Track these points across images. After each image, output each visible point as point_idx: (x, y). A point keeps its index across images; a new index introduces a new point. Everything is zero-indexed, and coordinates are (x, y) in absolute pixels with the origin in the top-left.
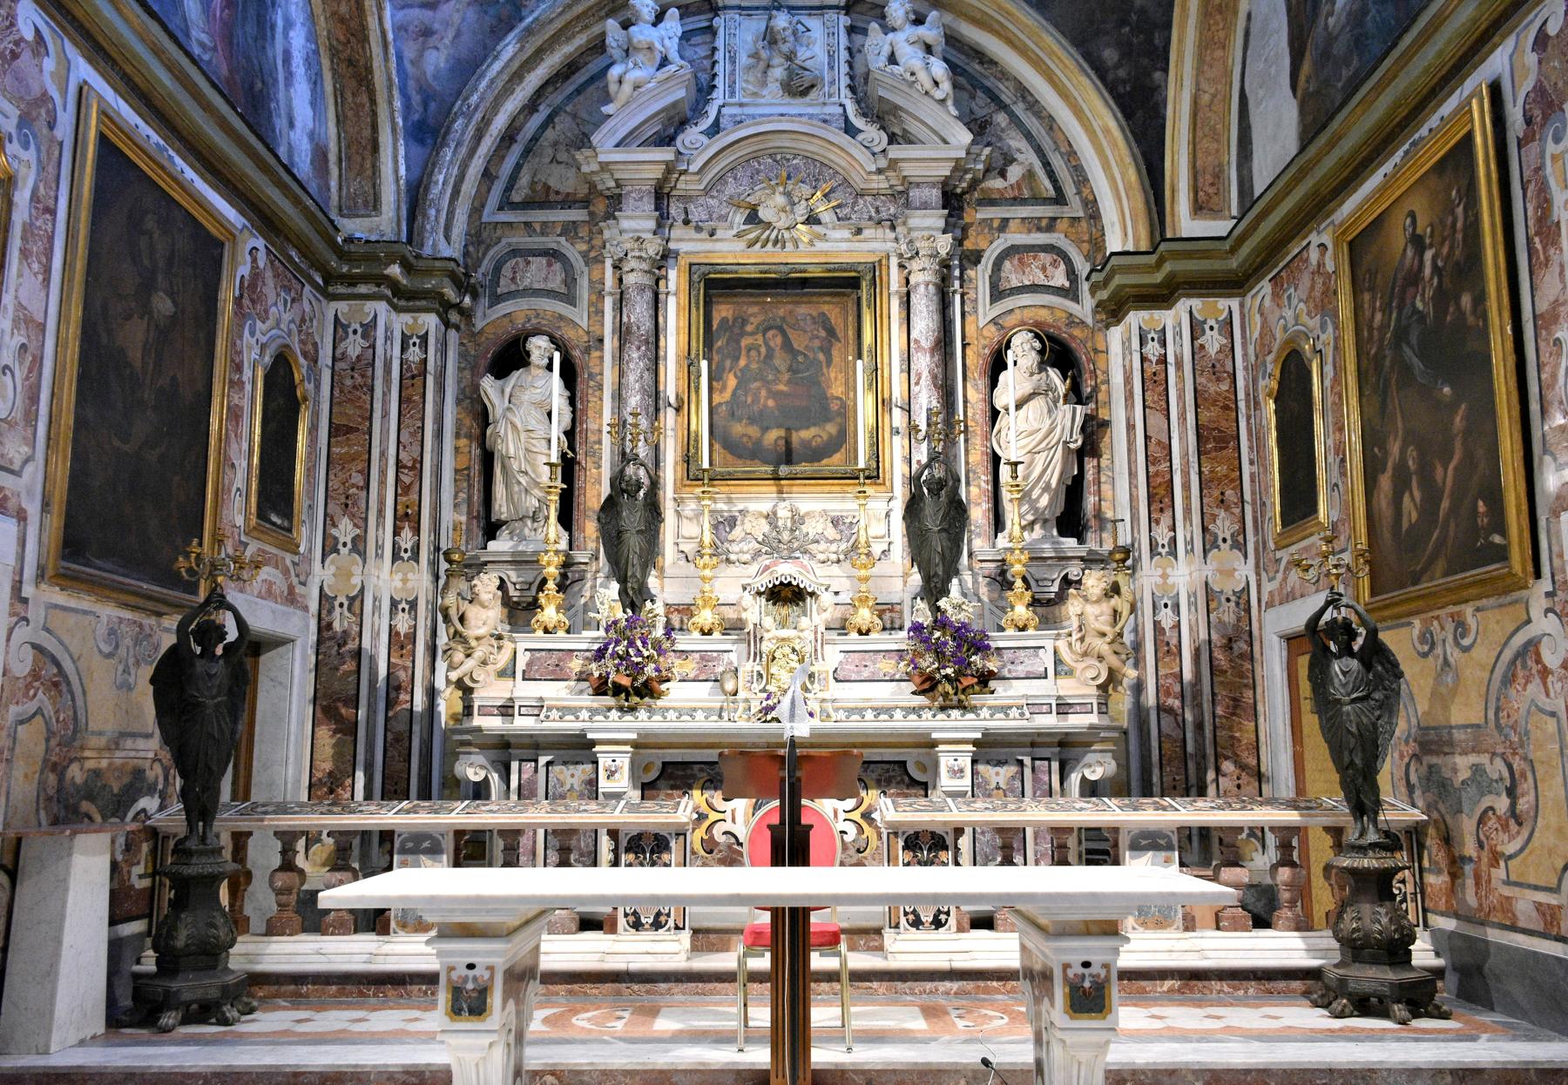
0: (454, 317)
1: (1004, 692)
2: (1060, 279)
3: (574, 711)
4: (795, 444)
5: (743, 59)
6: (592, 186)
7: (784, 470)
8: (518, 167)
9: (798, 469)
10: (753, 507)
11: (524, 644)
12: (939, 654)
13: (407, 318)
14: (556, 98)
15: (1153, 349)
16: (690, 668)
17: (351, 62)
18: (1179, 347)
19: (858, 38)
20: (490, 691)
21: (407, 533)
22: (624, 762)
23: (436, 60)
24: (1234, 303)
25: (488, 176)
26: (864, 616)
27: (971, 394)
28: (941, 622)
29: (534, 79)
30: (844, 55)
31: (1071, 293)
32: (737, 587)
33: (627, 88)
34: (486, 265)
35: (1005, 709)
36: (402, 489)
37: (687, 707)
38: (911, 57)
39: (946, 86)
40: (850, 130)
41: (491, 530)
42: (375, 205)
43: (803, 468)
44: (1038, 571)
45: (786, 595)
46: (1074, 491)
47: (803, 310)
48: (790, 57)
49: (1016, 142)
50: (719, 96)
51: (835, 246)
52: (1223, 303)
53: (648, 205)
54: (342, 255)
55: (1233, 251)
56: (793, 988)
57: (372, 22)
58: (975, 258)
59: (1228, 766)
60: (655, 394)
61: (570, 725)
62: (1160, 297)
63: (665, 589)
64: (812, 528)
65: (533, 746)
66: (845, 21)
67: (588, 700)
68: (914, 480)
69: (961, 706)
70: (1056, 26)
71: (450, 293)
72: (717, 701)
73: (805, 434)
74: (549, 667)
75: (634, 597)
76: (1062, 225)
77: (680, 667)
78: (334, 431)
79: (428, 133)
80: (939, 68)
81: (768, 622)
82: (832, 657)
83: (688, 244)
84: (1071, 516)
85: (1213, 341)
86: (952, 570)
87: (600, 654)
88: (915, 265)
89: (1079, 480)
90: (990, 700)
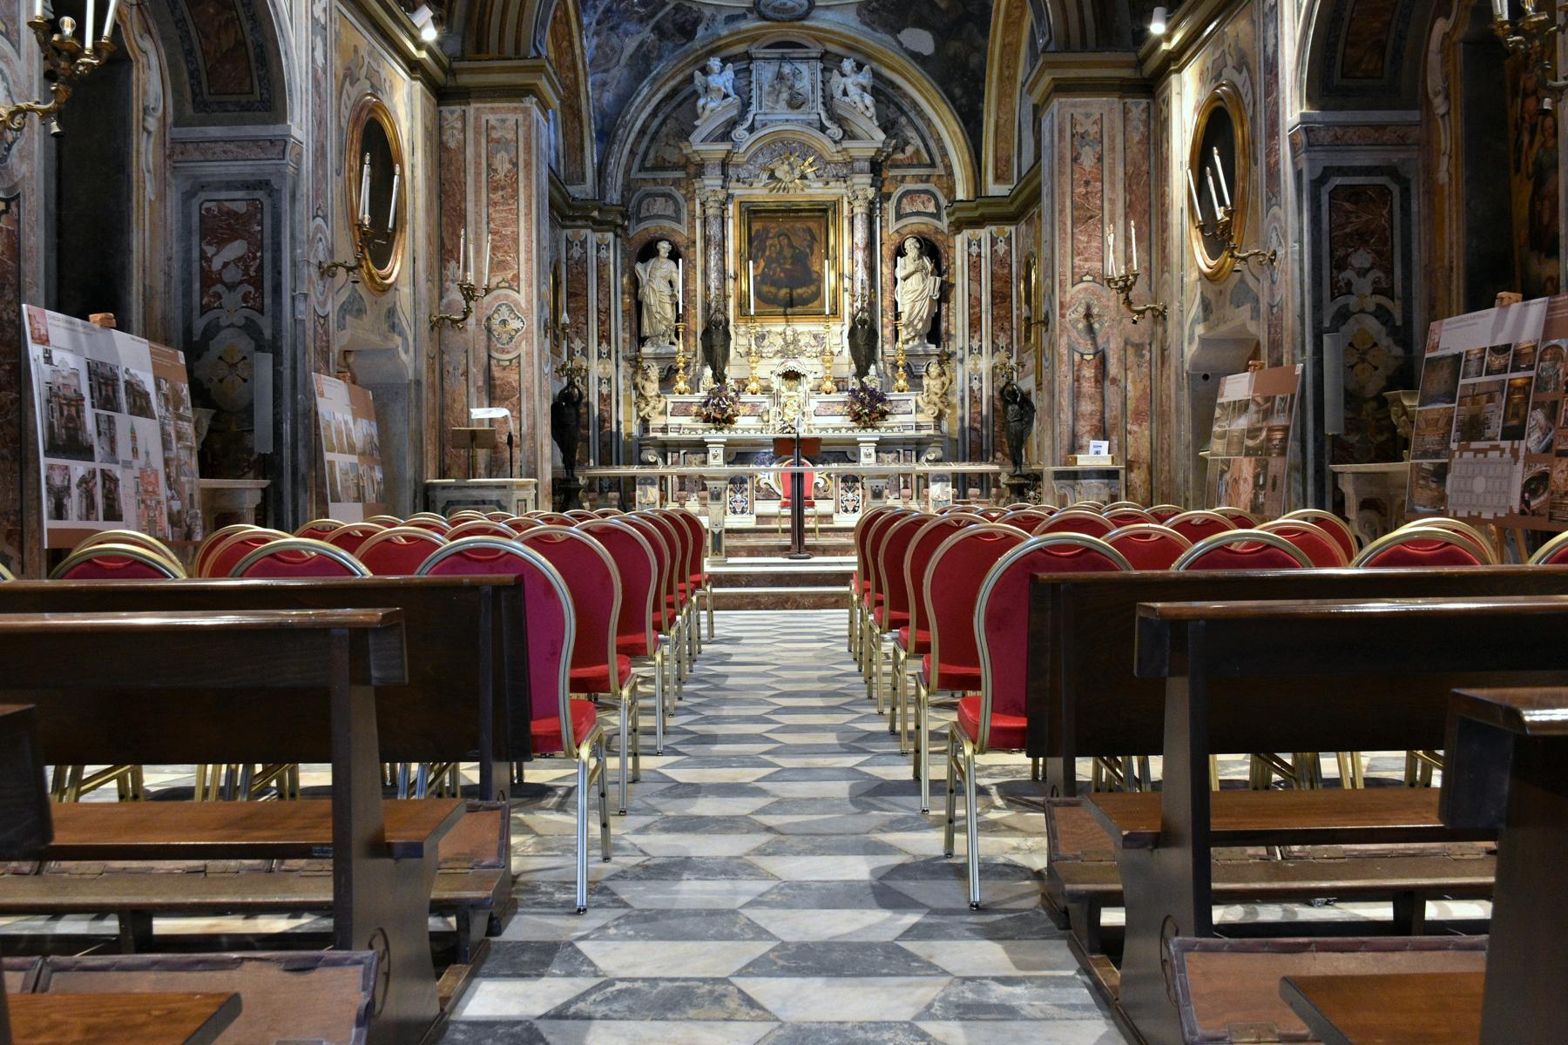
0: (619, 231)
1: (892, 421)
2: (931, 209)
3: (695, 430)
4: (791, 291)
5: (766, 88)
6: (688, 159)
7: (789, 310)
8: (648, 148)
9: (796, 309)
10: (774, 329)
11: (671, 399)
12: (862, 401)
13: (599, 235)
14: (668, 109)
15: (974, 249)
16: (747, 410)
17: (570, 107)
18: (986, 250)
19: (827, 74)
20: (657, 421)
21: (604, 345)
22: (721, 452)
23: (608, 97)
24: (1013, 228)
25: (632, 152)
26: (828, 385)
27: (883, 270)
28: (864, 388)
29: (655, 100)
30: (820, 85)
31: (937, 216)
32: (767, 369)
33: (707, 112)
34: (634, 202)
35: (891, 428)
36: (601, 323)
37: (746, 426)
38: (854, 92)
39: (872, 110)
40: (823, 129)
41: (642, 341)
42: (583, 180)
43: (798, 309)
44: (913, 361)
45: (792, 376)
46: (935, 320)
47: (798, 225)
48: (791, 87)
49: (911, 133)
50: (753, 109)
51: (817, 191)
52: (1007, 228)
53: (718, 172)
54: (570, 207)
55: (1011, 203)
56: (798, 530)
57: (582, 89)
58: (888, 197)
59: (999, 455)
60: (723, 272)
61: (694, 436)
62: (977, 223)
63: (732, 373)
64: (804, 340)
65: (678, 445)
66: (820, 66)
67: (701, 425)
68: (853, 317)
69: (873, 427)
70: (930, 73)
71: (619, 221)
72: (760, 425)
73: (800, 291)
74: (682, 410)
75: (719, 377)
76: (933, 179)
77: (742, 410)
78: (570, 295)
79: (606, 136)
80: (869, 100)
81: (783, 388)
82: (813, 404)
83: (738, 191)
84: (935, 332)
85: (1001, 248)
86: (871, 359)
87: (706, 404)
88: (856, 203)
89: (938, 315)
90: (885, 424)
